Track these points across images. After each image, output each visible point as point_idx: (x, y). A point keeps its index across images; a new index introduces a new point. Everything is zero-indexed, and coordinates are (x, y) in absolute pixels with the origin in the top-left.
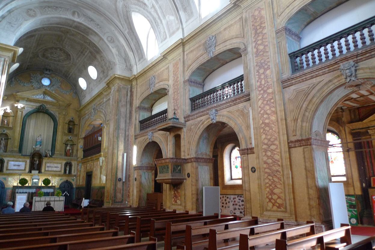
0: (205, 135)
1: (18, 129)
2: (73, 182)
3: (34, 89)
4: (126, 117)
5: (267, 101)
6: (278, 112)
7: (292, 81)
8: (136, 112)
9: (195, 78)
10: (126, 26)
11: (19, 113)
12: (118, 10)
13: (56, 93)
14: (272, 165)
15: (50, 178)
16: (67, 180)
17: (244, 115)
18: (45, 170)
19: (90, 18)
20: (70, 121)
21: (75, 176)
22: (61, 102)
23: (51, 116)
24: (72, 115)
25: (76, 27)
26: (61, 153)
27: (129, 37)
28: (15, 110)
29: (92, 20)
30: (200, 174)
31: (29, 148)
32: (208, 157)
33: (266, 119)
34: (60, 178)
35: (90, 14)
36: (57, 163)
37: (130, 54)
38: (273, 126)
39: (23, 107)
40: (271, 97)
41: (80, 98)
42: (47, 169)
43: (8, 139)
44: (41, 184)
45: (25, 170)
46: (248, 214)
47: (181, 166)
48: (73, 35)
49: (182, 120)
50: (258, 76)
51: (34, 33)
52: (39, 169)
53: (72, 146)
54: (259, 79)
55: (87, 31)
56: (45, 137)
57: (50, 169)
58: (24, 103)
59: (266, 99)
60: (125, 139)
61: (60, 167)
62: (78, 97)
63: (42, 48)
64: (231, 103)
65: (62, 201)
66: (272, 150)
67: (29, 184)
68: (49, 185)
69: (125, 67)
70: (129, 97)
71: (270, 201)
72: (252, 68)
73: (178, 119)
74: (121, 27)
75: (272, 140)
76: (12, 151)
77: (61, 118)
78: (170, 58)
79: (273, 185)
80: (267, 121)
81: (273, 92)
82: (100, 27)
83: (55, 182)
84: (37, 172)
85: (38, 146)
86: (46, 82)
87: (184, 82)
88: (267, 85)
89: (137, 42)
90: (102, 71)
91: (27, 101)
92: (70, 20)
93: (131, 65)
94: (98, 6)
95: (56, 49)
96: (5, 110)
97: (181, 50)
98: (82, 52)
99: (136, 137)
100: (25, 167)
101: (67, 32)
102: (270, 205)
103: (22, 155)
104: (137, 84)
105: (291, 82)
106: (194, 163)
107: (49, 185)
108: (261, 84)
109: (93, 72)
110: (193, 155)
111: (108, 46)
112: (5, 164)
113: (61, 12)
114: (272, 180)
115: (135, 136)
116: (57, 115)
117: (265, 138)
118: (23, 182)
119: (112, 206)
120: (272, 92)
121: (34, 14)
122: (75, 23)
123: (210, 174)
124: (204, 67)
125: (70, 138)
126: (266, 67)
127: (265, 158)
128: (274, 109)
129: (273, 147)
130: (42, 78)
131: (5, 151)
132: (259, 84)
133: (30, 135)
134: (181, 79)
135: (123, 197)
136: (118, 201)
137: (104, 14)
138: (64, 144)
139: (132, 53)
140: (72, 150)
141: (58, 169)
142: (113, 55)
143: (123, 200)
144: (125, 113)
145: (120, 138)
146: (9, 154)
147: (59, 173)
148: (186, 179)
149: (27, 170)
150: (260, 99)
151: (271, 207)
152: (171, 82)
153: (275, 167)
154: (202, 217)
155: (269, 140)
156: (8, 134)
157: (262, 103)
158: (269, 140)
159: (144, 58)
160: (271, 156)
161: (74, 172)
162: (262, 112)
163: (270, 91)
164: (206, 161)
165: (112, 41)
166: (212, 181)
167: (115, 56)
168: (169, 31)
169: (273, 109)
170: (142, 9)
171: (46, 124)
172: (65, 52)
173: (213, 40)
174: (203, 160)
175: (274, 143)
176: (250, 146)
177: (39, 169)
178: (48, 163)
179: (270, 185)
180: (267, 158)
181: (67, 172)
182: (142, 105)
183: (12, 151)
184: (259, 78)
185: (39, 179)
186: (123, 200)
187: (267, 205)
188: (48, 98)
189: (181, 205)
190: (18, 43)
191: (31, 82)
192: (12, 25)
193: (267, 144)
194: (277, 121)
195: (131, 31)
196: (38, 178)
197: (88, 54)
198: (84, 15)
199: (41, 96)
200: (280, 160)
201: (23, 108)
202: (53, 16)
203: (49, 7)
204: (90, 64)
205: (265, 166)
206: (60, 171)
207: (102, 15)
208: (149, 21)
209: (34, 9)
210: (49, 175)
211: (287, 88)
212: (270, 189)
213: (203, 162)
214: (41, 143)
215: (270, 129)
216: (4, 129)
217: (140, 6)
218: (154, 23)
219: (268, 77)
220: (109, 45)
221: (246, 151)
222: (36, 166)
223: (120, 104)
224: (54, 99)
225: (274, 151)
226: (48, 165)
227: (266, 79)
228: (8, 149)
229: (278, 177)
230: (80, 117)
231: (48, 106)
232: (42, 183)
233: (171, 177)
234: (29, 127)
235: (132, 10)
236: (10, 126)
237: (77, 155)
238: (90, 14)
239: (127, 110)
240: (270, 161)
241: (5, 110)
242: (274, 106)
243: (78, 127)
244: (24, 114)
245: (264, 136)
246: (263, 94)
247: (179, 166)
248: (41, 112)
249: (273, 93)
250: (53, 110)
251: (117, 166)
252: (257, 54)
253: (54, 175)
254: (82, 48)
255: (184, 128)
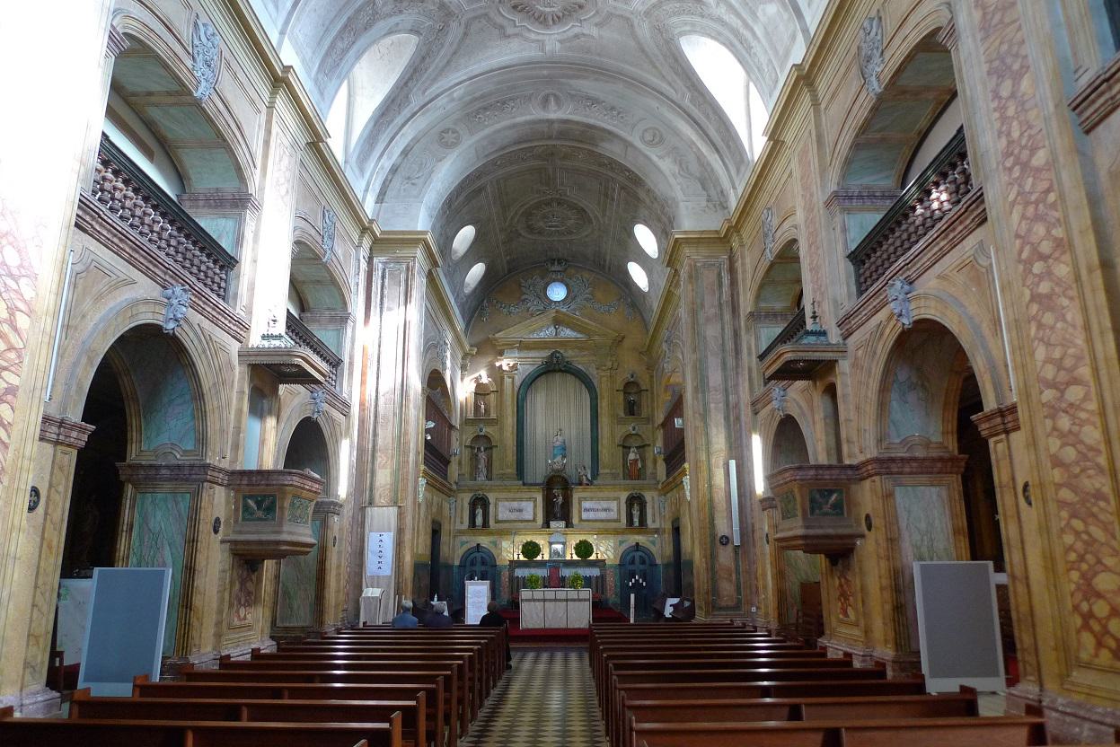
0: (903, 374)
1: (510, 421)
2: (654, 549)
3: (532, 315)
4: (723, 351)
5: (1037, 203)
6: (1077, 241)
7: (1110, 88)
8: (748, 329)
9: (857, 183)
10: (680, 83)
11: (508, 381)
12: (647, 49)
13: (582, 315)
14: (1077, 470)
15: (592, 539)
16: (637, 544)
17: (978, 275)
18: (581, 520)
19: (588, 99)
20: (628, 385)
21: (656, 531)
22: (596, 338)
23: (580, 379)
24: (631, 365)
25: (563, 135)
26: (614, 471)
27: (696, 111)
28: (497, 373)
29: (594, 101)
30: (902, 515)
31: (539, 467)
32: (935, 454)
33: (1041, 277)
34: (620, 538)
35: (587, 86)
36: (608, 499)
37: (714, 159)
38: (1065, 302)
39: (514, 365)
40: (1045, 185)
41: (645, 315)
42: (585, 516)
43: (491, 448)
44: (571, 555)
45: (534, 520)
46: (1031, 675)
47: (840, 492)
48: (565, 157)
49: (834, 336)
50: (997, 115)
51: (478, 184)
52: (566, 517)
53: (641, 450)
54: (1003, 124)
55: (589, 135)
56: (574, 432)
57: (591, 515)
58: (513, 355)
59: (1033, 198)
60: (727, 418)
61: (615, 510)
62: (641, 314)
63: (516, 213)
64: (942, 244)
65: (585, 600)
66: (1072, 405)
67: (545, 555)
68: (591, 558)
69: (704, 203)
70: (726, 289)
71: (1086, 626)
72: (979, 87)
73: (824, 333)
74: (672, 91)
75: (1068, 363)
76: (502, 477)
77: (605, 379)
78: (788, 137)
79: (1089, 557)
80: (1044, 288)
81: (1050, 161)
82: (619, 113)
83: (605, 550)
84: (562, 524)
85: (559, 458)
86: (557, 293)
87: (828, 204)
88: (1030, 137)
89: (720, 118)
90: (662, 232)
91: (520, 349)
92: (541, 121)
93: (722, 192)
94: (598, 58)
95: (548, 204)
96: (477, 380)
97: (806, 100)
98: (606, 195)
99: (756, 406)
100: (535, 514)
101: (550, 154)
102: (1088, 640)
103: (524, 484)
104: (742, 245)
105: (1107, 96)
106: (877, 478)
107: (591, 558)
108: (1010, 143)
109: (645, 237)
110: (872, 452)
111: (647, 157)
112: (492, 508)
113: (514, 109)
114: (1085, 537)
115: (753, 404)
116: (592, 372)
117: (1048, 360)
118: (531, 550)
119: (708, 620)
120: (1047, 163)
121: (455, 138)
122: (556, 126)
123: (953, 516)
124: (878, 136)
125: (634, 429)
126: (1016, 67)
127: (1054, 444)
128: (1060, 230)
129: (1074, 393)
130: (547, 284)
131: (489, 478)
132: (1004, 141)
133: (539, 431)
134: (820, 197)
135: (739, 593)
136: (723, 604)
137: (621, 74)
138: (619, 446)
139: (717, 156)
140: (643, 460)
141: (613, 515)
142: (666, 178)
143: (739, 601)
144: (720, 342)
145: (713, 416)
146: (498, 483)
147: (614, 525)
148: (863, 536)
149: (540, 520)
150: (1013, 203)
151: (1092, 651)
152: (800, 216)
153: (1089, 477)
154: (850, 669)
155: (1059, 364)
156: (489, 436)
157: (1023, 217)
158: (1059, 364)
159: (746, 160)
160: (1070, 431)
161: (654, 521)
162: (1024, 255)
163: (1040, 158)
164: (928, 468)
165: (657, 140)
166: (964, 543)
167: (672, 180)
168: (776, 52)
169: (1058, 232)
170: (699, 19)
171: (572, 395)
172: (573, 207)
173: (873, 34)
174: (914, 465)
175: (1076, 373)
176: (1008, 403)
177: (566, 517)
178: (585, 499)
179: (1082, 558)
180: (1058, 443)
181: (636, 520)
182: (763, 305)
183: (502, 477)
184: (1004, 119)
185: (564, 544)
186: (739, 601)
187: (1079, 641)
188: (567, 333)
189: (856, 625)
190: (453, 212)
191: (524, 300)
192: (413, 181)
193: (1053, 385)
194: (1078, 278)
195: (696, 94)
196: (563, 540)
197: (619, 194)
198: (572, 96)
199: (550, 330)
200: (1102, 447)
201: (514, 368)
202: (498, 126)
203: (485, 109)
204: (635, 221)
205: (1057, 475)
206: (618, 520)
207: (615, 78)
208: (724, 44)
209: (453, 127)
210: (590, 532)
211: (1101, 127)
212: (1083, 576)
213: (911, 473)
214: (564, 450)
215: (1057, 320)
216: (482, 426)
217: (691, 13)
218: (739, 46)
219: (1027, 106)
220: (648, 153)
221: (999, 420)
222: (557, 509)
223: (701, 317)
224: (579, 332)
225: (1079, 408)
226: (586, 504)
227: (1022, 118)
228: (496, 471)
229: (1102, 522)
230: (650, 367)
231: (569, 354)
232: (574, 552)
233: (800, 532)
234: (1097, 394)
235: (677, 31)
236: (493, 416)
237: (654, 475)
238: (587, 86)
239: (723, 329)
240: (1070, 454)
241: (477, 378)
242: (1058, 220)
243: (649, 395)
244: (518, 382)
245: (1041, 353)
246: (1019, 182)
247: (831, 492)
248: (554, 371)
249: (1052, 164)
250: (581, 361)
251: (711, 500)
252: (986, 28)
253: (603, 533)
254: (601, 184)
255: (840, 361)
